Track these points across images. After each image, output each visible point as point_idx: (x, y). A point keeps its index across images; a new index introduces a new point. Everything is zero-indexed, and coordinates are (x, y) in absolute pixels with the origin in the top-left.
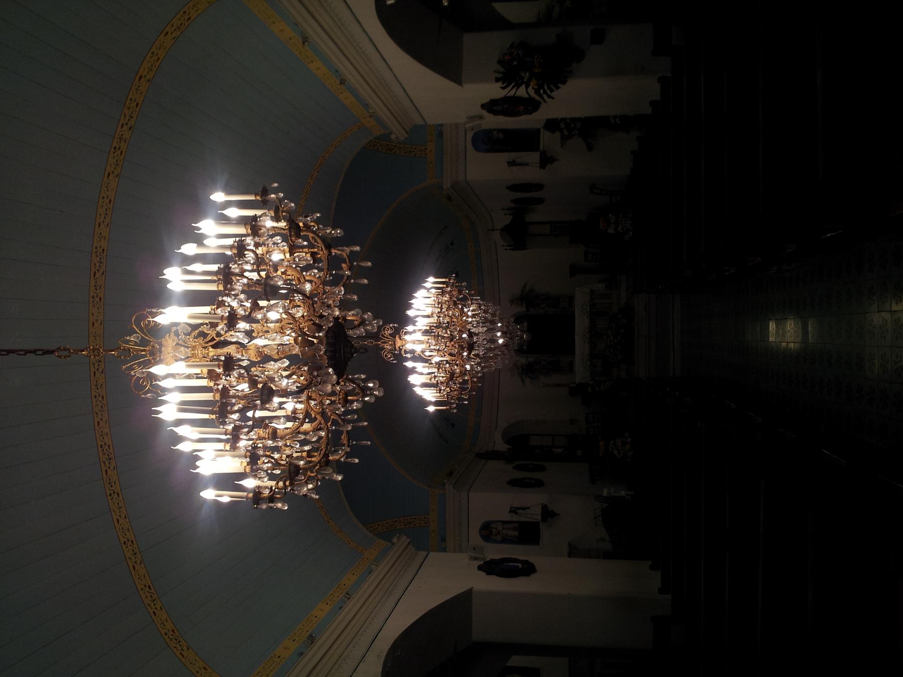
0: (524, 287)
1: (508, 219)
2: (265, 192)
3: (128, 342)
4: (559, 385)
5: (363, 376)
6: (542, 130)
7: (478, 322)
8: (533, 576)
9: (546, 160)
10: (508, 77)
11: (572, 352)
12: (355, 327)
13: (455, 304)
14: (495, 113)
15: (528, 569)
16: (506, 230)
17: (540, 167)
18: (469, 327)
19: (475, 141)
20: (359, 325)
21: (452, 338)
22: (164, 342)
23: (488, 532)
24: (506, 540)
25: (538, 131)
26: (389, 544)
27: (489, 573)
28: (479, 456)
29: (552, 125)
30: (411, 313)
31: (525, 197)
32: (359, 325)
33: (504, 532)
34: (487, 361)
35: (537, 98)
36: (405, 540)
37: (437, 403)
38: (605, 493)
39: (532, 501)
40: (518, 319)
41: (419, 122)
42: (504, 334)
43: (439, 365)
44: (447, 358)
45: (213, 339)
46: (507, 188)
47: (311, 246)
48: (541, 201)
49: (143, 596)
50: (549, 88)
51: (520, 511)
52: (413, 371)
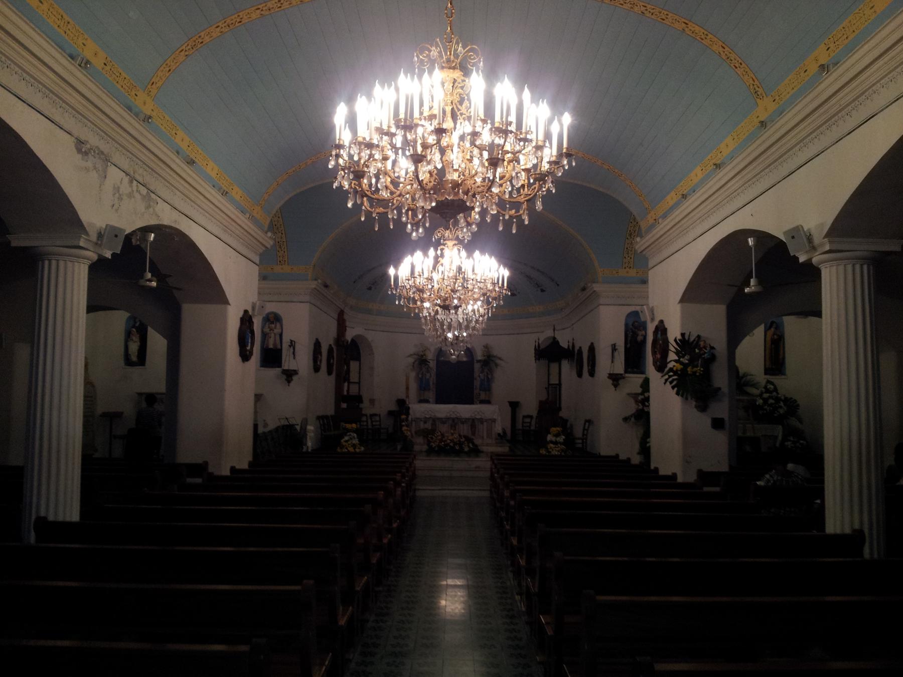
0: (500, 359)
1: (564, 344)
2: (568, 155)
3: (457, 43)
4: (407, 388)
5: (427, 225)
6: (644, 376)
7: (467, 314)
8: (239, 359)
9: (615, 379)
10: (685, 344)
11: (439, 401)
12: (465, 218)
13: (484, 295)
14: (656, 332)
15: (245, 356)
16: (555, 342)
17: (610, 374)
18: (463, 305)
19: (636, 314)
20: (467, 222)
21: (454, 291)
22: (456, 71)
23: (273, 319)
24: (265, 336)
25: (643, 372)
26: (266, 229)
27: (242, 319)
28: (341, 314)
29: (646, 385)
30: (477, 254)
31: (583, 360)
32: (467, 222)
33: (273, 335)
34: (431, 322)
35: (667, 369)
36: (269, 243)
37: (396, 278)
38: (310, 428)
39: (301, 361)
40: (469, 352)
41: (651, 265)
42: (456, 338)
43: (430, 279)
44: (436, 286)
45: (459, 110)
46: (592, 344)
47: (530, 185)
48: (580, 375)
49: (233, 17)
50: (674, 380)
51: (292, 350)
52: (426, 254)
